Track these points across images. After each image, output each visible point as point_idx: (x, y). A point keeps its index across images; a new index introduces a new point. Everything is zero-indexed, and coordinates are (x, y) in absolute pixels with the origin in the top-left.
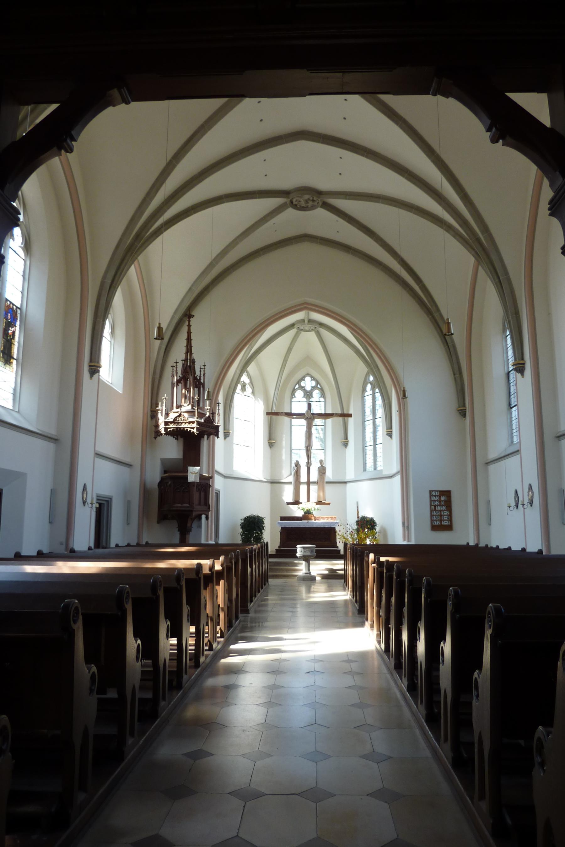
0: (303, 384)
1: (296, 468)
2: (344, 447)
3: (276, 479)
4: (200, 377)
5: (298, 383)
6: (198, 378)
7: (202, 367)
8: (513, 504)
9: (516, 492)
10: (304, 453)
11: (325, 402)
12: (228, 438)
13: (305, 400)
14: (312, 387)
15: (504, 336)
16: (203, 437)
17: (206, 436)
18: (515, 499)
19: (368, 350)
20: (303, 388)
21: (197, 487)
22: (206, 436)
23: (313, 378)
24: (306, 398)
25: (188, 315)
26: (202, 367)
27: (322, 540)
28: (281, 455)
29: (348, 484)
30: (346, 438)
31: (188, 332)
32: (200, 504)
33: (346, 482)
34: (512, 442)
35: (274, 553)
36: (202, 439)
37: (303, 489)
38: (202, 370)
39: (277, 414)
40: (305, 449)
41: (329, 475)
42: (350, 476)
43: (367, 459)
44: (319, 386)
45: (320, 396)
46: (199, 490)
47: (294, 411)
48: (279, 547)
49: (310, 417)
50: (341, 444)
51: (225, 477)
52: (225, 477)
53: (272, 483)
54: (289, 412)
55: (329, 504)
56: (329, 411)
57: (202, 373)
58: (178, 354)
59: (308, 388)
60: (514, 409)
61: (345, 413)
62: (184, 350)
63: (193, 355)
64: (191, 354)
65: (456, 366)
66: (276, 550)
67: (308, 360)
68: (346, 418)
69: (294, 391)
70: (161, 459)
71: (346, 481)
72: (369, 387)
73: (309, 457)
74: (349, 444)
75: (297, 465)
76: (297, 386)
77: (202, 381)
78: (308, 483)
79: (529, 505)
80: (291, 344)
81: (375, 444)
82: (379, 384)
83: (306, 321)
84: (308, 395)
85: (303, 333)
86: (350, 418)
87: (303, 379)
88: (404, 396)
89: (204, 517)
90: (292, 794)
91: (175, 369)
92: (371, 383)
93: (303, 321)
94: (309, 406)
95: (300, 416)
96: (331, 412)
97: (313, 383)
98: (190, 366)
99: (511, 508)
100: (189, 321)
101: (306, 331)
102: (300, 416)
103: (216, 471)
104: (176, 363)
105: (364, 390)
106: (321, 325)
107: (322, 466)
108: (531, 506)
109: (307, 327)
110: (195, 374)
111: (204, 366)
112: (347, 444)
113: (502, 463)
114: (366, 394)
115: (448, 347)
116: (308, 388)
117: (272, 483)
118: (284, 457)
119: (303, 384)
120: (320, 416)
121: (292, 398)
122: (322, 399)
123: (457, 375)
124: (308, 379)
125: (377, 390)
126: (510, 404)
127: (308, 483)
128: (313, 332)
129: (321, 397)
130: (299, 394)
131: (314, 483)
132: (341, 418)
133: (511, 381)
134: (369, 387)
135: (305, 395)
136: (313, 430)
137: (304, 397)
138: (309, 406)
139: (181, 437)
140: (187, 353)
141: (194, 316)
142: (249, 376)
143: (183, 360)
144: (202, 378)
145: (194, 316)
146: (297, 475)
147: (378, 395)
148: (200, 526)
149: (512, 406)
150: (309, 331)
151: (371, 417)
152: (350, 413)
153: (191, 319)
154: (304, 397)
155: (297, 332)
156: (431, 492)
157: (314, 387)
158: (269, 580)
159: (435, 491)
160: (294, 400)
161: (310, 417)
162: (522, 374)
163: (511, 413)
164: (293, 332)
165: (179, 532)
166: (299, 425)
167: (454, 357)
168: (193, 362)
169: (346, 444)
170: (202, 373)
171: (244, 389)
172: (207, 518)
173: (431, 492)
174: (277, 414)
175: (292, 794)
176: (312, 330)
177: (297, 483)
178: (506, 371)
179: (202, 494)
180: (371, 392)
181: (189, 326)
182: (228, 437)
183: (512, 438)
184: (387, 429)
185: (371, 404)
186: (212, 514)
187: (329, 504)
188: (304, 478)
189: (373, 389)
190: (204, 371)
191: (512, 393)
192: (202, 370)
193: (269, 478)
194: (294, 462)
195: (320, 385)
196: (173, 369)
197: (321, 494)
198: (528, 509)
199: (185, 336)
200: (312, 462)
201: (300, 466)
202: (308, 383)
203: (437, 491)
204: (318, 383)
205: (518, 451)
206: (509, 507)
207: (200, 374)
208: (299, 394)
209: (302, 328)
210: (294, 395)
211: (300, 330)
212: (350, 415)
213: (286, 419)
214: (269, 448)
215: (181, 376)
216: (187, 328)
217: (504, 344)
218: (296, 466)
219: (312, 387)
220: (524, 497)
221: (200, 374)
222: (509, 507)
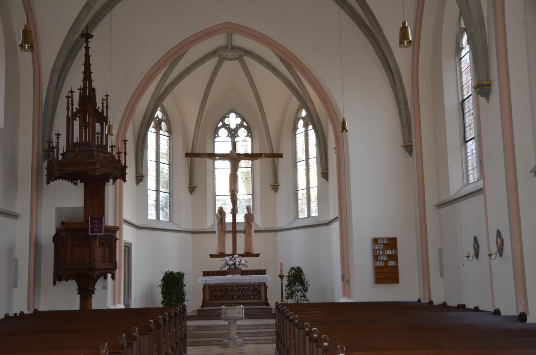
1: (220, 216)
2: (274, 192)
4: (103, 109)
5: (222, 120)
6: (100, 110)
7: (105, 98)
8: (472, 253)
9: (475, 239)
10: (228, 199)
11: (252, 141)
12: (141, 183)
13: (229, 139)
14: (237, 125)
15: (457, 59)
16: (108, 182)
17: (111, 181)
18: (474, 247)
19: (300, 80)
20: (226, 126)
21: (100, 241)
22: (111, 181)
23: (238, 115)
24: (230, 137)
25: (87, 36)
26: (105, 98)
27: (251, 296)
31: (85, 55)
32: (103, 261)
34: (468, 181)
35: (196, 314)
36: (107, 183)
38: (105, 102)
39: (198, 155)
40: (229, 194)
41: (258, 222)
43: (299, 204)
44: (245, 124)
45: (246, 134)
46: (102, 245)
47: (217, 151)
48: (202, 306)
49: (234, 158)
50: (271, 188)
54: (211, 152)
55: (258, 255)
56: (257, 152)
57: (105, 105)
58: (74, 81)
59: (233, 126)
60: (470, 143)
61: (275, 152)
62: (82, 77)
63: (93, 83)
64: (91, 82)
65: (401, 97)
66: (198, 310)
68: (276, 159)
69: (217, 129)
70: (57, 209)
72: (301, 123)
74: (280, 187)
75: (222, 212)
76: (221, 124)
77: (105, 114)
78: (234, 232)
79: (498, 255)
80: (212, 75)
82: (312, 120)
83: (229, 48)
84: (233, 134)
86: (280, 159)
87: (226, 115)
88: (344, 129)
89: (109, 275)
91: (70, 99)
92: (303, 119)
93: (224, 48)
94: (234, 145)
95: (223, 157)
96: (258, 153)
97: (239, 121)
98: (89, 96)
99: (470, 258)
100: (87, 42)
101: (229, 59)
102: (223, 157)
103: (125, 221)
104: (72, 92)
105: (295, 128)
106: (247, 52)
108: (501, 256)
109: (231, 54)
110: (96, 105)
111: (107, 96)
113: (456, 205)
114: (298, 132)
115: (392, 74)
116: (233, 126)
119: (226, 121)
120: (246, 156)
121: (215, 137)
122: (249, 139)
123: (403, 106)
124: (232, 115)
125: (310, 127)
126: (465, 138)
128: (237, 62)
129: (247, 136)
130: (223, 133)
131: (240, 232)
132: (270, 160)
133: (466, 111)
134: (301, 123)
135: (229, 133)
136: (239, 172)
137: (228, 136)
138: (234, 145)
139: (81, 182)
140: (84, 81)
141: (92, 36)
142: (164, 112)
143: (80, 89)
144: (105, 111)
145: (92, 36)
146: (222, 224)
147: (312, 134)
148: (105, 287)
149: (468, 139)
150: (233, 59)
151: (304, 158)
152: (280, 153)
153: (90, 40)
154: (228, 136)
155: (219, 61)
156: (376, 241)
157: (240, 125)
158: (188, 348)
159: (383, 239)
160: (217, 139)
161: (234, 158)
162: (488, 99)
163: (466, 148)
165: (79, 296)
166: (223, 168)
167: (398, 85)
168: (93, 91)
170: (105, 105)
171: (158, 127)
172: (113, 278)
173: (376, 241)
174: (198, 155)
176: (236, 59)
178: (460, 100)
179: (107, 249)
180: (303, 129)
181: (87, 48)
182: (141, 181)
183: (468, 176)
184: (322, 170)
185: (304, 142)
186: (120, 272)
187: (258, 255)
189: (306, 126)
190: (107, 102)
191: (467, 125)
192: (105, 102)
195: (246, 123)
196: (68, 100)
198: (497, 261)
199: (83, 60)
200: (238, 209)
201: (225, 214)
202: (233, 120)
203: (386, 239)
204: (243, 120)
205: (481, 190)
206: (468, 257)
207: (103, 107)
208: (223, 133)
209: (224, 56)
210: (217, 133)
212: (280, 156)
213: (209, 161)
214: (189, 194)
215: (78, 108)
216: (84, 50)
217: (458, 69)
219: (237, 125)
220: (489, 245)
221: (103, 107)
222: (468, 257)
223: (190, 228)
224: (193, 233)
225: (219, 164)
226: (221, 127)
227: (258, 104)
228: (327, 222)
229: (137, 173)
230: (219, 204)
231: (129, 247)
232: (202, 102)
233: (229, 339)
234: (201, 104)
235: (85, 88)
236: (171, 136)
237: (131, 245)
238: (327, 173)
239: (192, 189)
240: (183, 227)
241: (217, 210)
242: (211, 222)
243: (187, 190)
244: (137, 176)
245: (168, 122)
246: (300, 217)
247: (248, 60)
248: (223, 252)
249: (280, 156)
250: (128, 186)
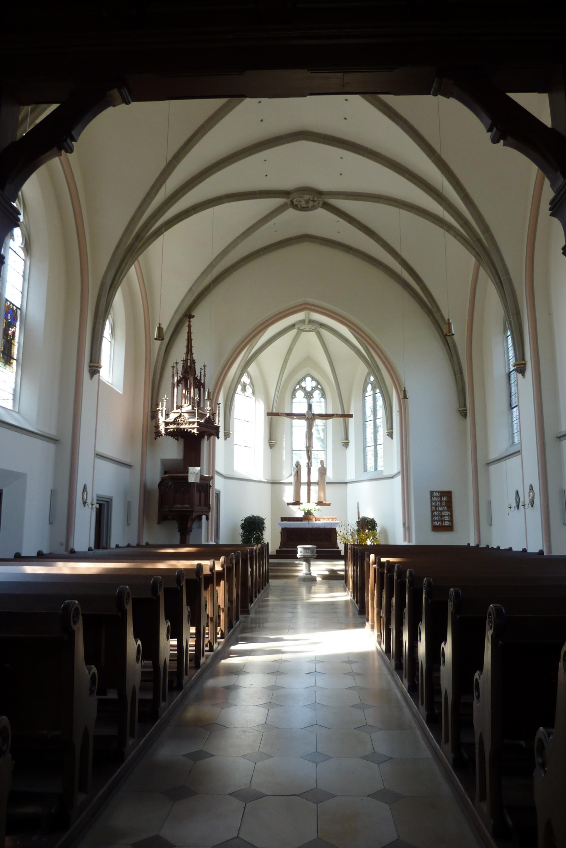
0: (303, 384)
1: (296, 469)
2: (344, 448)
3: (277, 479)
4: (200, 377)
5: (299, 383)
6: (199, 378)
7: (203, 368)
8: (514, 504)
9: (517, 492)
10: (304, 454)
11: (326, 402)
12: (228, 439)
13: (305, 400)
14: (313, 388)
15: (505, 337)
16: (204, 438)
17: (206, 437)
18: (516, 499)
19: (368, 350)
20: (303, 389)
21: (197, 488)
22: (206, 437)
23: (313, 379)
24: (306, 398)
25: (188, 315)
26: (203, 368)
27: (322, 541)
28: (282, 456)
29: (349, 485)
30: (347, 438)
31: (188, 333)
32: (200, 505)
33: (346, 483)
34: (513, 442)
35: (275, 554)
36: (202, 439)
37: (304, 489)
38: (203, 371)
39: (277, 414)
40: (305, 449)
41: (330, 476)
42: (351, 476)
43: (368, 460)
44: (319, 386)
45: (320, 396)
46: (199, 491)
47: (295, 411)
48: (280, 548)
49: (310, 418)
50: (342, 444)
51: (226, 477)
52: (226, 477)
53: (273, 483)
54: (289, 412)
55: (329, 505)
56: (330, 412)
57: (203, 374)
58: (178, 354)
59: (309, 389)
60: (515, 410)
61: (346, 413)
62: (184, 350)
63: (193, 356)
64: (192, 354)
65: (457, 367)
66: (277, 550)
67: (308, 360)
68: (346, 419)
69: (294, 391)
70: (161, 460)
71: (346, 481)
72: (369, 387)
73: (309, 457)
74: (350, 444)
75: (298, 465)
76: (298, 387)
77: (202, 381)
78: (309, 484)
79: (530, 506)
80: (291, 344)
81: (376, 445)
82: (380, 384)
83: (307, 322)
84: (309, 395)
85: (303, 333)
86: (350, 419)
87: (303, 379)
88: (405, 397)
89: (204, 517)
90: (293, 795)
91: (175, 369)
92: (372, 384)
93: (303, 321)
94: (310, 407)
95: (300, 416)
96: (331, 413)
97: (314, 384)
98: (190, 367)
99: (512, 509)
100: (190, 322)
101: (306, 331)
102: (300, 416)
103: (217, 472)
104: (177, 363)
105: (365, 391)
106: (322, 325)
107: (323, 466)
108: (532, 506)
109: (308, 327)
110: (195, 374)
111: (205, 366)
112: (348, 444)
113: (503, 463)
114: (367, 394)
115: (449, 347)
116: (309, 389)
117: (273, 483)
118: (284, 458)
119: (303, 384)
120: (321, 416)
121: (293, 398)
122: (323, 400)
123: (458, 376)
124: (308, 379)
125: (378, 391)
126: (511, 405)
127: (309, 484)
128: (314, 333)
129: (322, 397)
130: (300, 394)
131: (314, 483)
132: (341, 419)
133: (512, 382)
134: (369, 387)
135: (305, 395)
136: (314, 430)
137: (304, 397)
138: (310, 407)
139: (182, 438)
140: (187, 353)
141: (194, 316)
142: (250, 377)
143: (183, 361)
144: (202, 379)
145: (194, 316)
146: (298, 476)
147: (379, 396)
148: (200, 527)
149: (513, 406)
150: (310, 331)
151: (372, 418)
152: (351, 413)
153: (192, 320)
154: (304, 397)
155: (298, 332)
156: (432, 492)
157: (314, 387)
158: (270, 581)
159: (436, 492)
160: (294, 400)
161: (310, 418)
162: (523, 375)
163: (512, 414)
164: (293, 332)
165: (179, 533)
166: (300, 426)
167: (455, 358)
168: (193, 362)
169: (346, 445)
170: (203, 374)
171: (244, 389)
172: (207, 519)
173: (432, 492)
174: (277, 414)
175: (293, 795)
176: (313, 331)
177: (298, 483)
178: (507, 372)
179: (203, 495)
180: (372, 393)
181: (189, 326)
182: (229, 437)
183: (513, 438)
184: (388, 430)
185: (372, 405)
186: (212, 515)
187: (329, 505)
188: (304, 479)
189: (374, 389)
190: (205, 371)
191: (513, 394)
192: (203, 371)
193: (269, 478)
194: (294, 463)
195: (321, 386)
196: (173, 370)
197: (322, 495)
199: (186, 337)
200: (313, 463)
201: (300, 467)
202: (309, 384)
203: (438, 492)
204: (318, 383)
205: (519, 451)
206: (510, 508)
207: (201, 375)
208: (300, 394)
209: (302, 328)
210: (295, 395)
211: (300, 331)
212: (351, 416)
213: (287, 419)
214: (269, 448)
215: (181, 376)
216: (187, 328)
217: (505, 345)
218: (297, 466)
219: (313, 388)
220: (525, 498)
221: (201, 375)
222: (510, 508)
235: (186, 361)
237: (111, 499)
241: (19, 319)
250: (220, 443)
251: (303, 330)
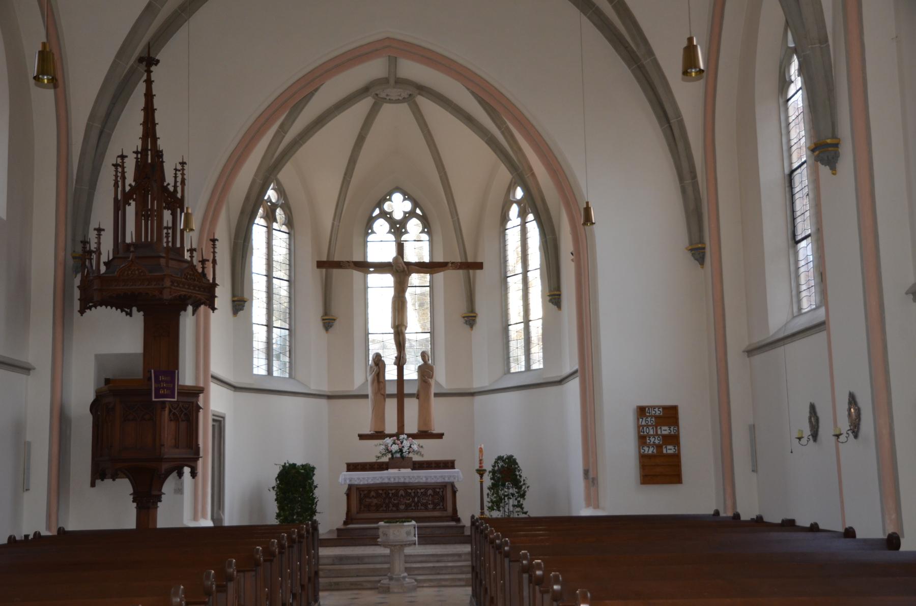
1: (376, 369)
2: (467, 327)
4: (175, 187)
5: (380, 204)
6: (171, 189)
7: (179, 167)
8: (807, 432)
9: (813, 408)
10: (390, 340)
11: (431, 241)
12: (241, 313)
13: (392, 237)
14: (405, 213)
15: (781, 101)
16: (185, 310)
17: (190, 308)
18: (810, 421)
19: (512, 136)
20: (387, 216)
21: (170, 411)
22: (190, 308)
23: (407, 196)
24: (394, 233)
25: (149, 61)
26: (179, 167)
31: (145, 95)
32: (176, 446)
34: (800, 309)
35: (334, 536)
36: (182, 313)
38: (179, 173)
39: (339, 265)
40: (392, 331)
41: (441, 379)
43: (511, 349)
44: (418, 211)
45: (421, 229)
46: (174, 418)
47: (371, 258)
48: (345, 523)
49: (401, 270)
50: (463, 320)
54: (361, 259)
55: (440, 436)
56: (439, 259)
57: (179, 179)
58: (127, 138)
59: (398, 216)
60: (803, 244)
61: (470, 260)
62: (139, 131)
63: (159, 142)
64: (155, 139)
65: (685, 165)
66: (338, 530)
68: (471, 271)
69: (371, 221)
70: (97, 356)
72: (514, 210)
74: (478, 320)
75: (379, 361)
76: (377, 212)
77: (179, 195)
78: (401, 396)
79: (851, 436)
80: (362, 129)
82: (534, 205)
83: (392, 81)
84: (398, 228)
86: (478, 271)
87: (386, 197)
88: (588, 219)
89: (187, 470)
91: (120, 169)
92: (518, 203)
93: (383, 82)
94: (400, 248)
95: (381, 267)
96: (442, 260)
97: (408, 206)
98: (152, 164)
99: (804, 441)
100: (149, 72)
101: (391, 101)
102: (381, 267)
103: (213, 377)
104: (123, 157)
105: (505, 218)
106: (422, 89)
108: (856, 437)
109: (394, 93)
110: (163, 179)
111: (183, 163)
113: (780, 350)
114: (509, 225)
115: (670, 127)
116: (398, 216)
119: (387, 206)
120: (421, 267)
121: (367, 234)
122: (425, 237)
123: (688, 181)
124: (397, 197)
125: (531, 217)
126: (794, 235)
128: (405, 105)
129: (423, 232)
130: (381, 226)
131: (411, 395)
132: (461, 272)
133: (796, 190)
134: (514, 210)
135: (391, 228)
136: (409, 294)
137: (390, 232)
138: (400, 248)
139: (139, 311)
140: (144, 138)
141: (158, 61)
142: (280, 191)
143: (136, 152)
144: (179, 189)
145: (158, 61)
146: (379, 382)
147: (533, 229)
148: (179, 490)
149: (799, 238)
150: (398, 101)
151: (519, 269)
152: (479, 260)
153: (153, 68)
154: (390, 232)
155: (375, 104)
156: (642, 411)
157: (409, 213)
158: (321, 594)
159: (654, 407)
160: (370, 238)
161: (401, 270)
162: (833, 169)
163: (796, 253)
165: (135, 505)
166: (380, 287)
167: (681, 145)
168: (158, 155)
170: (179, 179)
171: (270, 218)
172: (194, 474)
173: (642, 411)
174: (339, 265)
176: (404, 100)
178: (787, 171)
179: (183, 425)
180: (518, 221)
181: (149, 82)
182: (242, 309)
183: (799, 301)
184: (550, 291)
185: (519, 243)
186: (205, 464)
187: (440, 436)
189: (522, 214)
190: (183, 174)
191: (798, 213)
192: (179, 173)
195: (421, 210)
196: (116, 171)
199: (142, 103)
200: (408, 356)
201: (384, 365)
202: (398, 205)
203: (659, 407)
204: (416, 204)
205: (822, 324)
206: (800, 439)
207: (176, 182)
208: (381, 226)
209: (383, 95)
210: (371, 228)
212: (479, 266)
213: (357, 274)
214: (323, 331)
215: (133, 184)
216: (144, 85)
217: (783, 118)
219: (405, 213)
220: (835, 418)
221: (176, 182)
222: (800, 439)
223: (325, 388)
224: (329, 397)
225: (374, 279)
226: (378, 217)
227: (441, 177)
228: (559, 379)
229: (233, 295)
230: (373, 349)
231: (220, 421)
232: (345, 174)
233: (391, 579)
234: (344, 178)
235: (144, 150)
236: (292, 233)
237: (224, 418)
238: (560, 295)
239: (328, 323)
240: (313, 388)
242: (360, 379)
243: (320, 324)
244: (233, 301)
245: (287, 208)
246: (512, 370)
247: (424, 102)
248: (381, 430)
249: (479, 266)
251: (384, 100)
